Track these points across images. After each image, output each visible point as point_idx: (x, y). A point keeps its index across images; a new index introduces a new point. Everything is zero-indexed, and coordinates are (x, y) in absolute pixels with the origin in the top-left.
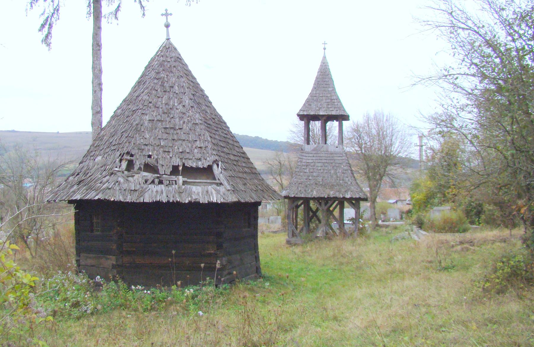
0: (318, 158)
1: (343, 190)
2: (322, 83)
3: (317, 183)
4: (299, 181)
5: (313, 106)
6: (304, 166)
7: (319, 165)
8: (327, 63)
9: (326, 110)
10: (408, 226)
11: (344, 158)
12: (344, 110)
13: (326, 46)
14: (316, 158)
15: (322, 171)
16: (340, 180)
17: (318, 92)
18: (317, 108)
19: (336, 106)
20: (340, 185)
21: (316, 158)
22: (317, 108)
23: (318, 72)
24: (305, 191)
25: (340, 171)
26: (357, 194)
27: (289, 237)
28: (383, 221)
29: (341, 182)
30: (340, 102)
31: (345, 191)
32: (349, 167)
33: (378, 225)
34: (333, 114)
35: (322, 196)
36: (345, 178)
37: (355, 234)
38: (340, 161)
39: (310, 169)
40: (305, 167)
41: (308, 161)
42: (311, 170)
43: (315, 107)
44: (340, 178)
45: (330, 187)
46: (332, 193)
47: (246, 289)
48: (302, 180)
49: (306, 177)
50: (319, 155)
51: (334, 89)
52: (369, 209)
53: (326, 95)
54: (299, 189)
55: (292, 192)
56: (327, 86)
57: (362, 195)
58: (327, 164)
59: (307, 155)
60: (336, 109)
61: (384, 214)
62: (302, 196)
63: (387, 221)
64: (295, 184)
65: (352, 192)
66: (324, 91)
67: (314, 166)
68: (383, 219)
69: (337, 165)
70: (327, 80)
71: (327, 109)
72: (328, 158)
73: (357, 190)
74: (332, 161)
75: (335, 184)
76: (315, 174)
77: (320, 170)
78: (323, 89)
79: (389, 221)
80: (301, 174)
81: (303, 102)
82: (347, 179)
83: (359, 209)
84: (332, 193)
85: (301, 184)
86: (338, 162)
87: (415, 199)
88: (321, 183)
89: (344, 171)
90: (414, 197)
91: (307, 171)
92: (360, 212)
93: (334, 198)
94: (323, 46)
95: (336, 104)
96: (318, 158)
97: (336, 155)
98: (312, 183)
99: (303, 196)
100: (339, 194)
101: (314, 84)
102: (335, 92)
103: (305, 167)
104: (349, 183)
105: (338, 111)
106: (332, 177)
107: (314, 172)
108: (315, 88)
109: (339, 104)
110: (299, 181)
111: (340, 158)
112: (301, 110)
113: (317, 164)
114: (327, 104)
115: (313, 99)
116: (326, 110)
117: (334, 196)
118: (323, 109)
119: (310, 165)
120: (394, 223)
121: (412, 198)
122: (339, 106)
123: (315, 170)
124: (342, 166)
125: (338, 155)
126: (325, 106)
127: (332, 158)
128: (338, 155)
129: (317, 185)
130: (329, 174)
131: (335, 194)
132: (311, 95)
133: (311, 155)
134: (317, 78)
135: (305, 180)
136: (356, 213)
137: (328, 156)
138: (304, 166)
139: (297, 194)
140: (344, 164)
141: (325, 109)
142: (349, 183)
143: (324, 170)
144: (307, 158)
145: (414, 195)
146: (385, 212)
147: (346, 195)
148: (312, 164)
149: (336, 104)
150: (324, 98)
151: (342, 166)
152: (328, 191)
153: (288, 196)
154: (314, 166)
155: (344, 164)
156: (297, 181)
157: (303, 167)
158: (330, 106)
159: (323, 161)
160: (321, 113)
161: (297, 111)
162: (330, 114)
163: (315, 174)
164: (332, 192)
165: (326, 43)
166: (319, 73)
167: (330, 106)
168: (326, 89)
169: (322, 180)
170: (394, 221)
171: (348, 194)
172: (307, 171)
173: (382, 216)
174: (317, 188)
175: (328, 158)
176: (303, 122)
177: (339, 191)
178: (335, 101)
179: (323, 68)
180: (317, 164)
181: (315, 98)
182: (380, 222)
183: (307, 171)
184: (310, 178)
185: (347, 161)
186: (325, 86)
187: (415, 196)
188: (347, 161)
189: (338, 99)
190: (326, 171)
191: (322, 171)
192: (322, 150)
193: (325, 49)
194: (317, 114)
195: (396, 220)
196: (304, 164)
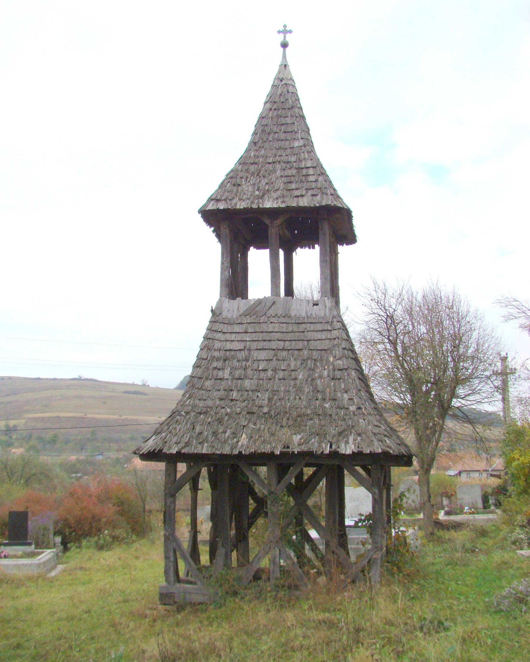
0: (261, 336)
1: (333, 431)
2: (275, 129)
3: (255, 409)
4: (201, 404)
5: (247, 188)
6: (218, 359)
7: (263, 355)
8: (291, 79)
9: (283, 196)
10: (518, 529)
11: (335, 333)
12: (335, 195)
13: (289, 37)
14: (254, 336)
15: (270, 373)
16: (324, 399)
17: (262, 152)
18: (257, 193)
19: (313, 185)
20: (325, 415)
21: (254, 336)
22: (257, 193)
23: (266, 103)
24: (215, 433)
25: (326, 373)
26: (376, 443)
27: (167, 580)
28: (448, 513)
29: (327, 405)
30: (323, 173)
31: (340, 434)
32: (353, 362)
33: (438, 524)
34: (301, 204)
35: (267, 449)
36: (339, 395)
37: (375, 573)
38: (326, 345)
39: (234, 369)
40: (219, 364)
41: (229, 346)
42: (237, 373)
43: (250, 189)
44: (323, 392)
45: (291, 422)
46: (297, 438)
47: (193, 641)
48: (210, 403)
49: (222, 393)
50: (264, 327)
51: (308, 144)
52: (417, 487)
53: (284, 159)
54: (198, 429)
55: (175, 440)
56: (289, 136)
57: (394, 449)
58: (284, 353)
59: (229, 329)
60: (310, 192)
61: (449, 497)
62: (204, 451)
63: (456, 514)
64: (187, 413)
65: (359, 435)
66: (280, 148)
67: (247, 360)
68: (446, 509)
69: (315, 355)
70: (289, 120)
71: (285, 193)
72: (289, 337)
73: (376, 430)
74: (300, 345)
75: (309, 412)
76: (247, 384)
77: (265, 370)
78: (276, 145)
79: (461, 512)
80: (208, 383)
81: (221, 177)
82: (346, 396)
83: (388, 491)
84: (297, 438)
85: (206, 413)
86: (318, 345)
87: (514, 464)
88: (266, 410)
89: (338, 374)
90: (514, 459)
91: (226, 374)
92: (392, 500)
93: (302, 454)
94: (280, 38)
95: (312, 178)
96: (261, 336)
97: (312, 327)
98: (238, 410)
99: (205, 450)
100: (320, 443)
101: (255, 134)
102: (312, 151)
103: (219, 364)
104: (353, 408)
105: (318, 198)
106: (299, 390)
107: (246, 377)
108: (255, 143)
109: (321, 179)
110: (201, 404)
111: (323, 335)
112: (211, 199)
113: (255, 355)
114: (288, 179)
115: (247, 171)
116: (283, 196)
117: (304, 448)
118: (275, 195)
119: (233, 357)
120: (471, 517)
121: (508, 463)
122: (319, 186)
123: (249, 372)
124: (331, 359)
125: (319, 327)
126: (282, 186)
127: (301, 336)
128: (319, 327)
129: (254, 418)
130: (292, 383)
131: (307, 442)
132: (243, 162)
133: (237, 328)
134: (262, 117)
135: (218, 402)
136: (376, 502)
137: (290, 329)
138: (218, 359)
139: (187, 444)
140: (338, 352)
141: (279, 193)
142: (353, 408)
143: (275, 370)
144: (228, 337)
145: (512, 455)
146: (450, 492)
147: (343, 445)
148: (241, 355)
149: (312, 178)
150: (278, 166)
151: (331, 359)
152: (284, 434)
153: (161, 451)
154: (247, 360)
155: (338, 352)
156: (195, 406)
157: (215, 364)
158: (293, 186)
159: (274, 345)
160: (268, 204)
161: (201, 201)
162: (294, 205)
163: (247, 384)
164: (299, 437)
165: (288, 29)
166: (268, 106)
167: (293, 186)
168: (287, 143)
169: (270, 400)
170: (473, 513)
171: (347, 442)
172: (226, 376)
173: (445, 502)
174: (251, 425)
175: (289, 337)
176: (270, 295)
177: (321, 435)
178: (311, 171)
179: (279, 92)
180: (255, 355)
181: (252, 168)
182: (442, 516)
183: (226, 374)
184: (234, 395)
185: (344, 344)
186: (282, 136)
187: (516, 456)
188: (344, 344)
189: (318, 167)
190: (281, 374)
191: (270, 373)
192: (272, 312)
193: (285, 45)
194: (255, 206)
195: (475, 511)
196: (216, 354)
